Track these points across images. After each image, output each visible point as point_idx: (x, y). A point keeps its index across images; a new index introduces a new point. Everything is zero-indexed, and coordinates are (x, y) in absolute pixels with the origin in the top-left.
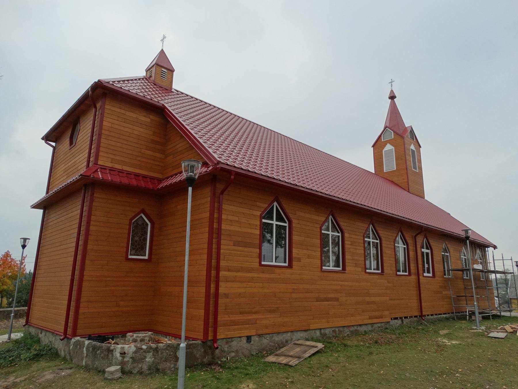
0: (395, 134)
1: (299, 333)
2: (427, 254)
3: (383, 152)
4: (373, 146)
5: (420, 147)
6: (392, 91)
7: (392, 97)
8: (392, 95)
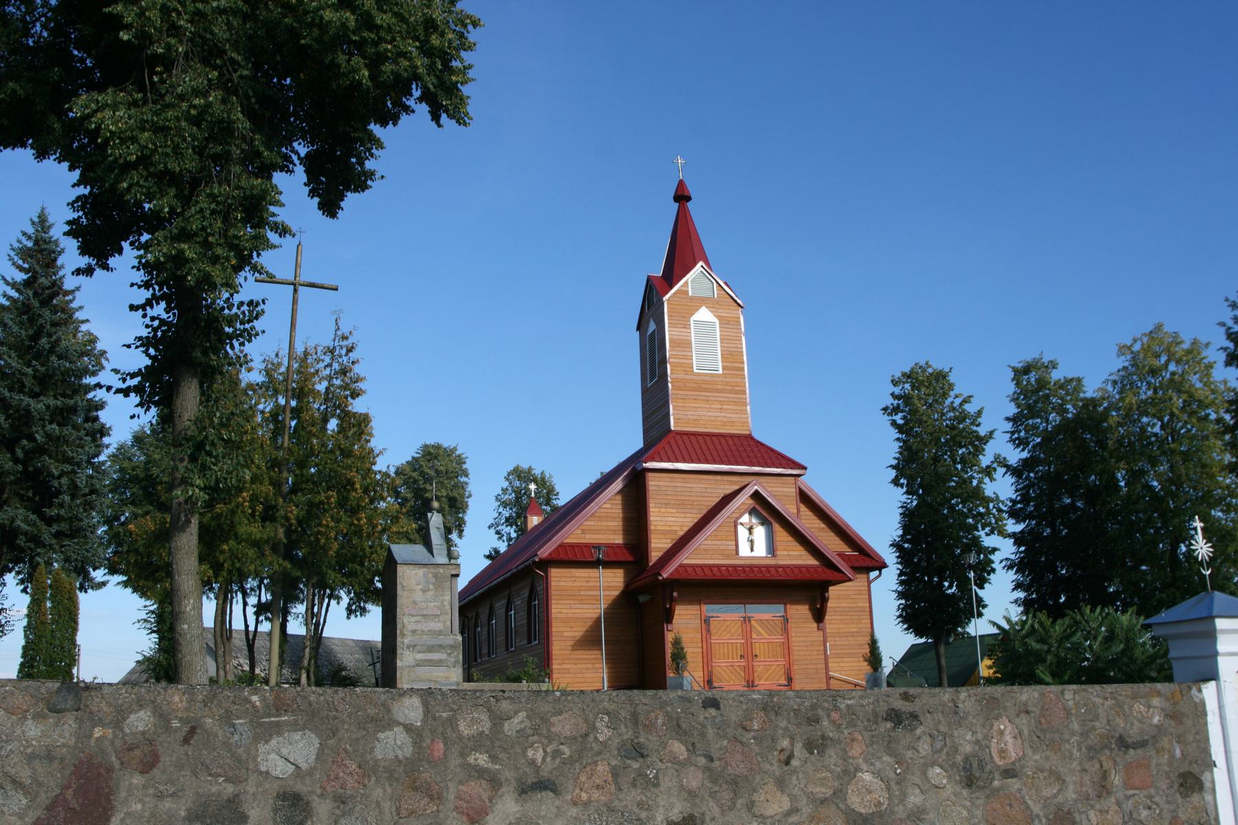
7: (682, 197)
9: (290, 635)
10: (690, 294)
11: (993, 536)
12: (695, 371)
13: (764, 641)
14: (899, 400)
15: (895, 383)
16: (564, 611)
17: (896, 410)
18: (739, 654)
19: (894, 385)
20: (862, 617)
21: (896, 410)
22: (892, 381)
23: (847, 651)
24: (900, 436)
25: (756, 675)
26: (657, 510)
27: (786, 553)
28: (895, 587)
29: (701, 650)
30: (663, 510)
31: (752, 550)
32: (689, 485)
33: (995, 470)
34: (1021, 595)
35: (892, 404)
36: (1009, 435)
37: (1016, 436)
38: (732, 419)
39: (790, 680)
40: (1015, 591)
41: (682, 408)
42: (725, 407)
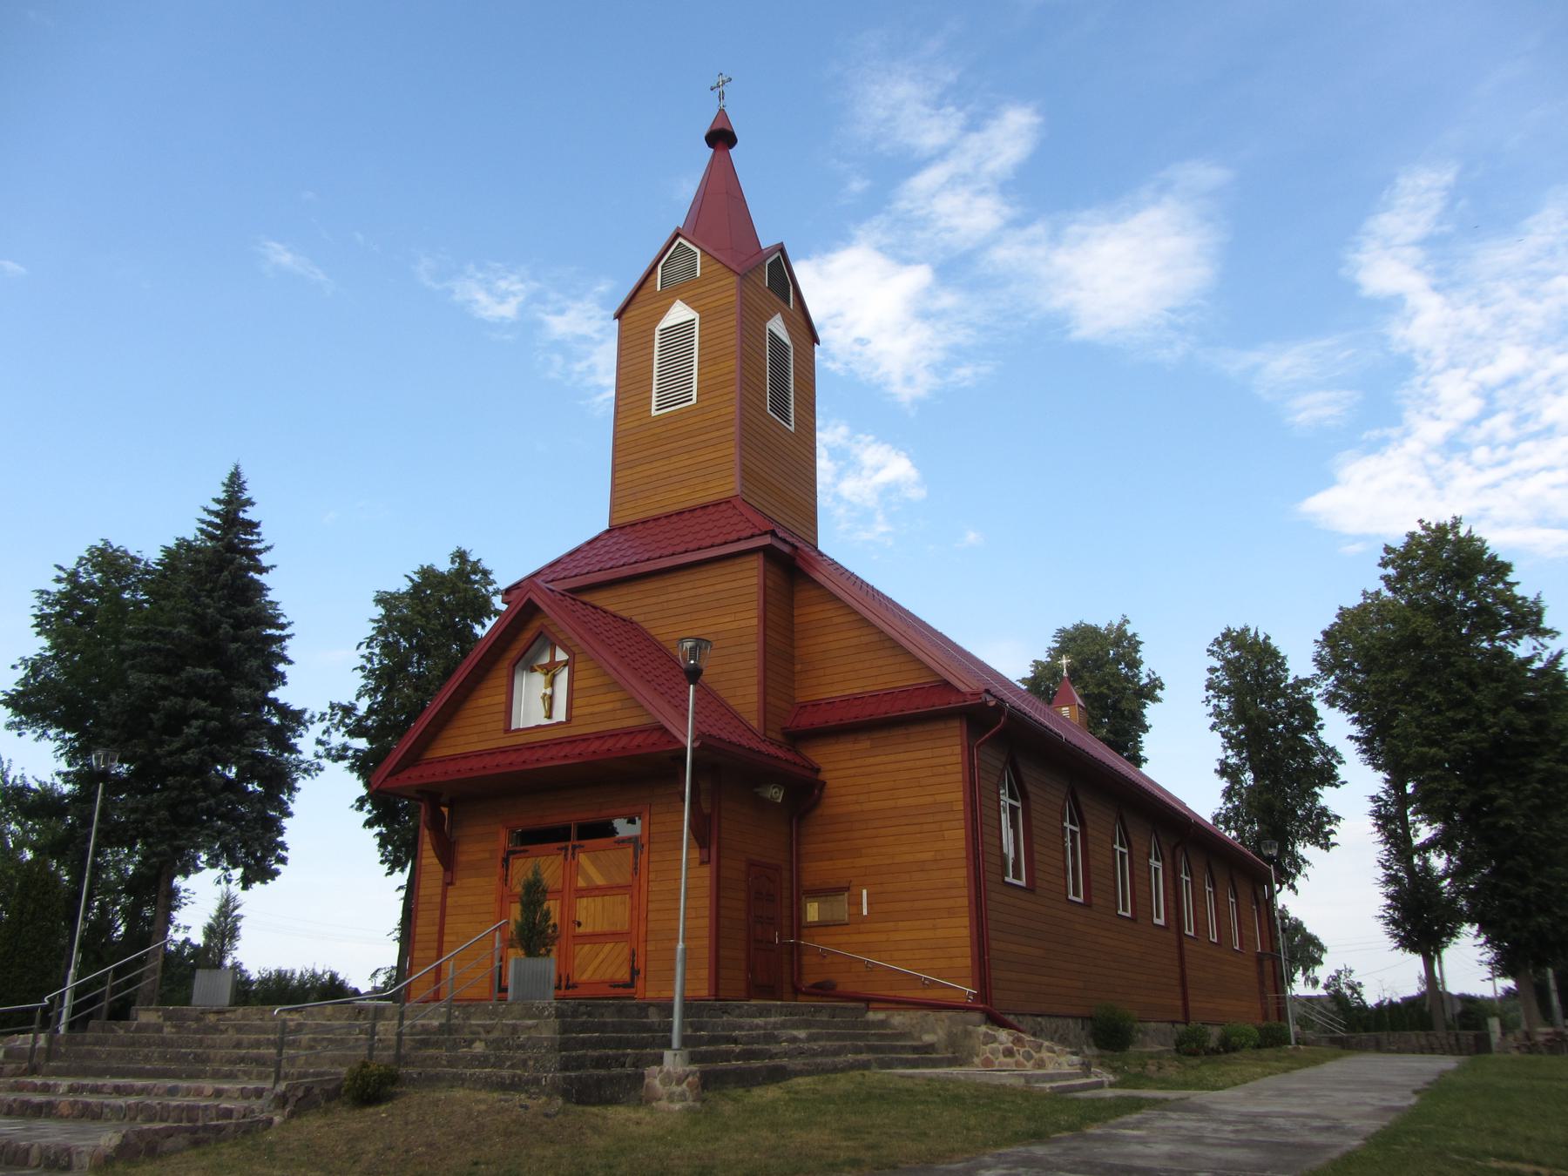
0: (708, 258)
1: (1543, 474)
2: (1122, 854)
3: (657, 333)
4: (619, 316)
5: (815, 340)
6: (722, 114)
7: (721, 138)
8: (718, 126)
39: (634, 972)
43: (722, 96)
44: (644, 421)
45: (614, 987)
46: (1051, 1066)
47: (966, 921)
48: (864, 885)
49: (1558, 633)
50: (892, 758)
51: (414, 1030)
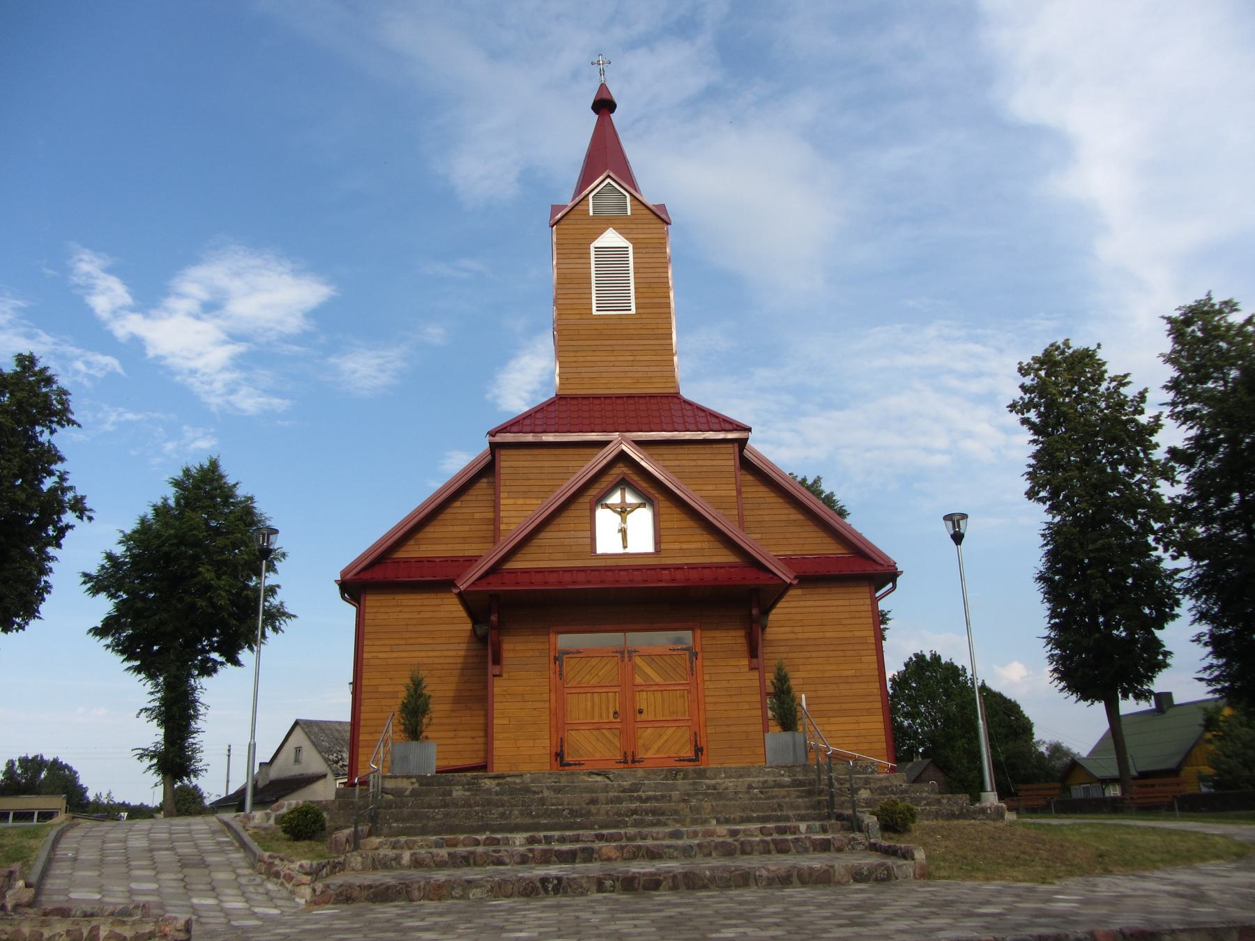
0: (636, 202)
6: (603, 87)
7: (604, 105)
9: (1093, 752)
10: (591, 214)
11: (1182, 558)
12: (594, 312)
13: (656, 688)
14: (1031, 393)
15: (1023, 371)
16: (381, 655)
17: (1027, 406)
18: (612, 712)
19: (1024, 375)
20: (862, 653)
21: (1027, 406)
22: (1020, 370)
23: (836, 707)
24: (1036, 437)
25: (640, 742)
26: (511, 501)
27: (677, 546)
28: (1046, 633)
29: (547, 705)
30: (520, 501)
31: (625, 547)
32: (565, 464)
33: (1173, 468)
34: (1205, 628)
35: (1022, 398)
36: (1170, 408)
37: (1179, 408)
38: (650, 374)
39: (699, 750)
40: (1196, 624)
41: (574, 365)
42: (638, 358)
43: (602, 72)
44: (585, 316)
45: (680, 760)
46: (817, 826)
47: (881, 718)
48: (802, 691)
49: (74, 526)
50: (819, 603)
51: (766, 785)
